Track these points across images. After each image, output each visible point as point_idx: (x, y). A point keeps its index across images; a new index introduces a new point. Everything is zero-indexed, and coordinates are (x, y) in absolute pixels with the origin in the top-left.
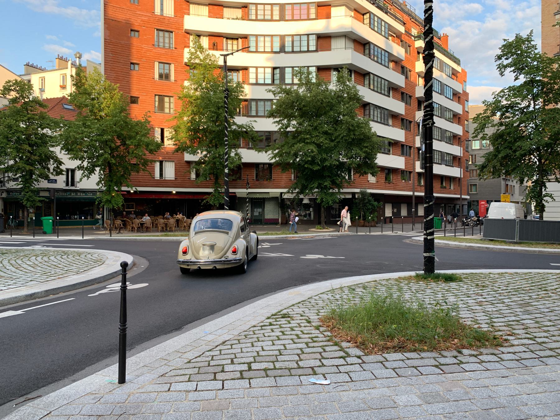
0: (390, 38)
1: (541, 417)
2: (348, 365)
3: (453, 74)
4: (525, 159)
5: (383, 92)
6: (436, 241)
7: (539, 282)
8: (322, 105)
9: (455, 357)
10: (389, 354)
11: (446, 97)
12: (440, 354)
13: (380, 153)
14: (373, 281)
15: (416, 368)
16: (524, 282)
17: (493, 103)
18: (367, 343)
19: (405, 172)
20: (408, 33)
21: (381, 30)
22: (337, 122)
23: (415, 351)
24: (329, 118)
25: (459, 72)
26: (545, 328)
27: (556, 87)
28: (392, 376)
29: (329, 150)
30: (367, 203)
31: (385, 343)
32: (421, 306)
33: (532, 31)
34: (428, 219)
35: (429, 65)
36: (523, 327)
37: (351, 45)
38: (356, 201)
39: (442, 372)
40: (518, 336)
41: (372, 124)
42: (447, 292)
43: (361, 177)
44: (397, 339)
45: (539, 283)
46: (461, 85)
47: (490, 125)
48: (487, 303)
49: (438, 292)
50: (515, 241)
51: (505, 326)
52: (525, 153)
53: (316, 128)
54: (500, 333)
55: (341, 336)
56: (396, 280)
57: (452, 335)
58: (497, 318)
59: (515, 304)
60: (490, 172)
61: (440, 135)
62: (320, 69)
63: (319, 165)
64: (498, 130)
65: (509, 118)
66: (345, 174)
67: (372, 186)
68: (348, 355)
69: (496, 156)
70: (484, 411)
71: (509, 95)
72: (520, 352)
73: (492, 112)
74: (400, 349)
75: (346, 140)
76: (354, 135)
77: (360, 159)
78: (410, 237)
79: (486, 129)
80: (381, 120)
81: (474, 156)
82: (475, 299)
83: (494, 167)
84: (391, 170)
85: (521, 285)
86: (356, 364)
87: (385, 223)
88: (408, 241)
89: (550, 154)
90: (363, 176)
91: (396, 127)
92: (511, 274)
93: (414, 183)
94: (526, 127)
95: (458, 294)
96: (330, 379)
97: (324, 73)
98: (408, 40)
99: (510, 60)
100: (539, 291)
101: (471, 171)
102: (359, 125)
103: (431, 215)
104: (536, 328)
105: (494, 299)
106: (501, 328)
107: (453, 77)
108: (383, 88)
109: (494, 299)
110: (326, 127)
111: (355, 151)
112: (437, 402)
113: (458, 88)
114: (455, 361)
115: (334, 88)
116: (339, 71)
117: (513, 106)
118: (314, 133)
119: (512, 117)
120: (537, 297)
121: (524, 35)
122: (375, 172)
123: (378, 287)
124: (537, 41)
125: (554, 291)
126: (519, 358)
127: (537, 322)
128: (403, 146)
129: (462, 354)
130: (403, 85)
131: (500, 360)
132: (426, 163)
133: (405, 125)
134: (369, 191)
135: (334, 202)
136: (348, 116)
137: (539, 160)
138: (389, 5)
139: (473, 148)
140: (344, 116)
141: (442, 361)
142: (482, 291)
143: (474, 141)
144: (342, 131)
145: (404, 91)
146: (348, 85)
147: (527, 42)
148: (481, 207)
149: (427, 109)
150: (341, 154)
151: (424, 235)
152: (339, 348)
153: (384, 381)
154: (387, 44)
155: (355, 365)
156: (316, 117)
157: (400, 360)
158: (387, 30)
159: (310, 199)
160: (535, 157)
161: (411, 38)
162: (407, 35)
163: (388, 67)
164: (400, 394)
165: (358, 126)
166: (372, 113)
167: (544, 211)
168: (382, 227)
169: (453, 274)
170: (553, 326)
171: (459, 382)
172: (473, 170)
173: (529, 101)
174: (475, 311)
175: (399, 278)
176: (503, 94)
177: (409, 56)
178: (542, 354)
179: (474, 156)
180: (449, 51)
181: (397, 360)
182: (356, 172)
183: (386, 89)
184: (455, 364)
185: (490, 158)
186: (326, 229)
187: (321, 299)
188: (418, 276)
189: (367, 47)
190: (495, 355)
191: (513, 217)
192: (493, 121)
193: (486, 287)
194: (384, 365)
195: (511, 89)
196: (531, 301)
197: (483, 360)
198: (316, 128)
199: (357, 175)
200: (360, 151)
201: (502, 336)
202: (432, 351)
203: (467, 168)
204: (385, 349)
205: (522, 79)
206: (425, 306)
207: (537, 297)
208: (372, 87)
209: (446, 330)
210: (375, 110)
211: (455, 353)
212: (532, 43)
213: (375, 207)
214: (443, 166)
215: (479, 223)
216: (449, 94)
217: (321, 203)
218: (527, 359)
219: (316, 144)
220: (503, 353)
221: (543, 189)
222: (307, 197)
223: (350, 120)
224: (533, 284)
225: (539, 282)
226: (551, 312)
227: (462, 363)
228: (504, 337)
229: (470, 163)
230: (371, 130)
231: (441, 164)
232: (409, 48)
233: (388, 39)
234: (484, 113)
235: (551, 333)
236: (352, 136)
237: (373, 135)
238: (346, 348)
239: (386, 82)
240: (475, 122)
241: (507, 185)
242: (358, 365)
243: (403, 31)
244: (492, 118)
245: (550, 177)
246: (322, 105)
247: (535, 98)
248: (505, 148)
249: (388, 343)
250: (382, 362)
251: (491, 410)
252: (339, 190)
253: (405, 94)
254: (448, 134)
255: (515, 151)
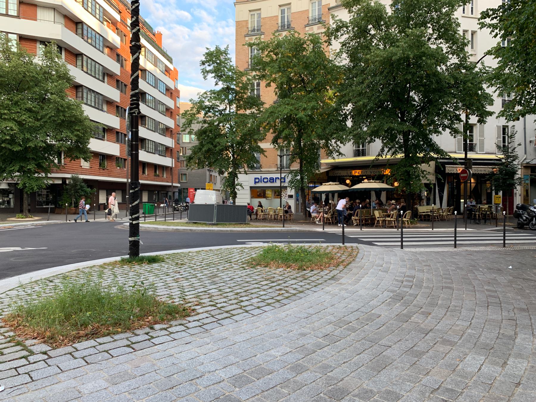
0: (105, 23)
1: (213, 371)
2: (30, 364)
3: (166, 71)
4: (223, 154)
5: (97, 76)
6: (140, 225)
7: (226, 256)
8: (24, 79)
9: (147, 334)
10: (80, 344)
11: (159, 91)
12: (133, 333)
13: (93, 138)
14: (76, 270)
15: (107, 351)
16: (215, 257)
17: (199, 103)
18: (57, 336)
19: (120, 159)
21: (96, 13)
22: (43, 100)
23: (108, 334)
24: (33, 94)
25: (172, 70)
26: (225, 295)
27: (245, 96)
28: (81, 366)
29: (33, 130)
30: (79, 189)
31: (77, 332)
32: (121, 289)
33: (228, 46)
34: (134, 204)
35: (135, 56)
36: (208, 296)
37: (62, 20)
38: (67, 187)
39: (133, 350)
40: (204, 305)
41: (84, 107)
42: (148, 273)
43: (72, 161)
44: (91, 326)
45: (226, 257)
46: (173, 82)
47: (196, 121)
48: (183, 279)
49: (141, 274)
50: (214, 222)
51: (194, 297)
52: (223, 148)
53: (16, 103)
54: (189, 305)
55: (26, 334)
56: (101, 266)
57: (148, 313)
58: (190, 291)
59: (205, 277)
60: (196, 163)
61: (154, 126)
62: (22, 38)
63: (20, 145)
64: (202, 127)
65: (211, 117)
66: (54, 157)
67: (85, 172)
68: (32, 353)
69: (200, 149)
70: (166, 379)
71: (211, 98)
72: (203, 319)
73: (197, 110)
74: (93, 336)
75: (55, 120)
76: (65, 116)
77: (71, 142)
78: (122, 223)
79: (192, 125)
80: (95, 105)
81: (184, 149)
82: (172, 277)
83: (199, 159)
84: (106, 156)
85: (213, 260)
86: (40, 361)
87: (99, 210)
88: (119, 227)
89: (241, 151)
90: (74, 160)
91: (111, 114)
92: (207, 251)
93: (127, 170)
94: (223, 126)
95: (158, 274)
96: (5, 385)
97: (28, 44)
98: (124, 29)
99: (211, 67)
100: (225, 264)
101: (182, 162)
102: (69, 107)
103: (136, 200)
104: (218, 295)
105: (189, 274)
106: (191, 300)
107: (166, 73)
108: (97, 72)
109: (189, 274)
110: (29, 104)
111: (66, 133)
112: (124, 381)
113: (171, 84)
114: (147, 337)
115: (40, 63)
116: (46, 45)
117: (214, 107)
118: (14, 109)
119: (213, 117)
120: (223, 269)
121: (223, 48)
122: (88, 158)
123: (79, 276)
124: (232, 56)
125: (236, 263)
126: (202, 324)
127: (220, 290)
128: (118, 133)
129: (154, 329)
130: (118, 73)
131: (186, 328)
132: (132, 150)
133: (120, 112)
134: (82, 177)
135: (40, 188)
136: (57, 95)
137: (233, 155)
139: (184, 141)
140: (52, 94)
141: (134, 339)
142: (180, 269)
143: (184, 135)
144: (49, 111)
145: (119, 79)
146: (56, 62)
147: (224, 54)
148: (190, 194)
149: (134, 98)
150: (48, 136)
151: (130, 219)
152: (22, 348)
153: (71, 373)
154: (101, 28)
155: (39, 363)
156: (17, 91)
157: (91, 347)
158: (101, 14)
159: (9, 184)
160: (230, 153)
161: (127, 28)
162: (123, 24)
163: (103, 52)
164: (87, 382)
165: (68, 108)
166: (85, 96)
167: (236, 197)
168: (95, 214)
169: (157, 256)
170: (231, 291)
171: (148, 356)
172: (183, 161)
173: (226, 105)
174: (171, 288)
175: (104, 264)
176: (206, 95)
177: (125, 46)
178: (219, 317)
179: (184, 149)
180: (162, 48)
181: (89, 348)
182: (66, 156)
183: (101, 74)
184: (146, 340)
185: (196, 150)
186: (30, 217)
187: (8, 297)
188: (123, 260)
189: (80, 26)
190: (182, 325)
191: (214, 203)
192: (198, 118)
193: (184, 264)
194: (73, 356)
195: (213, 92)
196: (218, 272)
197: (172, 331)
198: (16, 103)
199: (68, 159)
200: (71, 135)
201: (191, 306)
202: (126, 332)
203: (178, 158)
204: (78, 338)
205: (221, 85)
206: (124, 289)
207: (223, 269)
209: (141, 310)
210: (89, 93)
211: (147, 330)
212: (228, 56)
213: (88, 194)
214: (157, 155)
215: (186, 208)
216: (163, 89)
217: (23, 189)
218: (208, 323)
219: (16, 121)
220: (189, 322)
221: (236, 180)
222: (5, 181)
223: (59, 100)
224: (222, 258)
225: (226, 256)
226: (232, 280)
227: (152, 337)
228: (192, 308)
229: (181, 154)
230: (83, 113)
231: (154, 153)
232: (124, 37)
233: (103, 23)
234: (191, 110)
235: (229, 298)
236: (62, 118)
237: (85, 119)
238: (31, 346)
239: (101, 68)
240: (184, 118)
241: (211, 175)
242: (43, 362)
244: (198, 115)
245: (241, 170)
246: (24, 79)
247: (230, 103)
248: (208, 143)
249: (81, 332)
250: (70, 354)
251: (172, 376)
252: (46, 174)
253: (120, 82)
254: (161, 126)
255: (215, 146)
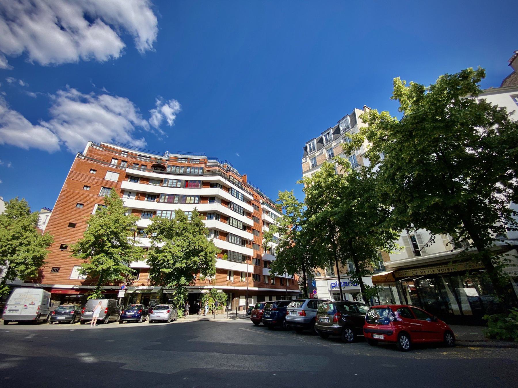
20: (257, 201)
138: (243, 186)
208: (231, 224)
243: (253, 199)
